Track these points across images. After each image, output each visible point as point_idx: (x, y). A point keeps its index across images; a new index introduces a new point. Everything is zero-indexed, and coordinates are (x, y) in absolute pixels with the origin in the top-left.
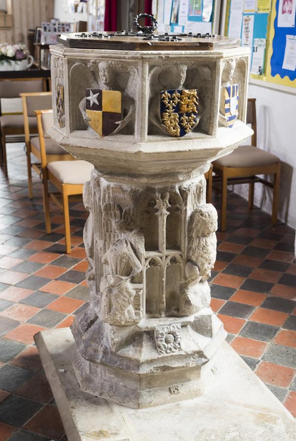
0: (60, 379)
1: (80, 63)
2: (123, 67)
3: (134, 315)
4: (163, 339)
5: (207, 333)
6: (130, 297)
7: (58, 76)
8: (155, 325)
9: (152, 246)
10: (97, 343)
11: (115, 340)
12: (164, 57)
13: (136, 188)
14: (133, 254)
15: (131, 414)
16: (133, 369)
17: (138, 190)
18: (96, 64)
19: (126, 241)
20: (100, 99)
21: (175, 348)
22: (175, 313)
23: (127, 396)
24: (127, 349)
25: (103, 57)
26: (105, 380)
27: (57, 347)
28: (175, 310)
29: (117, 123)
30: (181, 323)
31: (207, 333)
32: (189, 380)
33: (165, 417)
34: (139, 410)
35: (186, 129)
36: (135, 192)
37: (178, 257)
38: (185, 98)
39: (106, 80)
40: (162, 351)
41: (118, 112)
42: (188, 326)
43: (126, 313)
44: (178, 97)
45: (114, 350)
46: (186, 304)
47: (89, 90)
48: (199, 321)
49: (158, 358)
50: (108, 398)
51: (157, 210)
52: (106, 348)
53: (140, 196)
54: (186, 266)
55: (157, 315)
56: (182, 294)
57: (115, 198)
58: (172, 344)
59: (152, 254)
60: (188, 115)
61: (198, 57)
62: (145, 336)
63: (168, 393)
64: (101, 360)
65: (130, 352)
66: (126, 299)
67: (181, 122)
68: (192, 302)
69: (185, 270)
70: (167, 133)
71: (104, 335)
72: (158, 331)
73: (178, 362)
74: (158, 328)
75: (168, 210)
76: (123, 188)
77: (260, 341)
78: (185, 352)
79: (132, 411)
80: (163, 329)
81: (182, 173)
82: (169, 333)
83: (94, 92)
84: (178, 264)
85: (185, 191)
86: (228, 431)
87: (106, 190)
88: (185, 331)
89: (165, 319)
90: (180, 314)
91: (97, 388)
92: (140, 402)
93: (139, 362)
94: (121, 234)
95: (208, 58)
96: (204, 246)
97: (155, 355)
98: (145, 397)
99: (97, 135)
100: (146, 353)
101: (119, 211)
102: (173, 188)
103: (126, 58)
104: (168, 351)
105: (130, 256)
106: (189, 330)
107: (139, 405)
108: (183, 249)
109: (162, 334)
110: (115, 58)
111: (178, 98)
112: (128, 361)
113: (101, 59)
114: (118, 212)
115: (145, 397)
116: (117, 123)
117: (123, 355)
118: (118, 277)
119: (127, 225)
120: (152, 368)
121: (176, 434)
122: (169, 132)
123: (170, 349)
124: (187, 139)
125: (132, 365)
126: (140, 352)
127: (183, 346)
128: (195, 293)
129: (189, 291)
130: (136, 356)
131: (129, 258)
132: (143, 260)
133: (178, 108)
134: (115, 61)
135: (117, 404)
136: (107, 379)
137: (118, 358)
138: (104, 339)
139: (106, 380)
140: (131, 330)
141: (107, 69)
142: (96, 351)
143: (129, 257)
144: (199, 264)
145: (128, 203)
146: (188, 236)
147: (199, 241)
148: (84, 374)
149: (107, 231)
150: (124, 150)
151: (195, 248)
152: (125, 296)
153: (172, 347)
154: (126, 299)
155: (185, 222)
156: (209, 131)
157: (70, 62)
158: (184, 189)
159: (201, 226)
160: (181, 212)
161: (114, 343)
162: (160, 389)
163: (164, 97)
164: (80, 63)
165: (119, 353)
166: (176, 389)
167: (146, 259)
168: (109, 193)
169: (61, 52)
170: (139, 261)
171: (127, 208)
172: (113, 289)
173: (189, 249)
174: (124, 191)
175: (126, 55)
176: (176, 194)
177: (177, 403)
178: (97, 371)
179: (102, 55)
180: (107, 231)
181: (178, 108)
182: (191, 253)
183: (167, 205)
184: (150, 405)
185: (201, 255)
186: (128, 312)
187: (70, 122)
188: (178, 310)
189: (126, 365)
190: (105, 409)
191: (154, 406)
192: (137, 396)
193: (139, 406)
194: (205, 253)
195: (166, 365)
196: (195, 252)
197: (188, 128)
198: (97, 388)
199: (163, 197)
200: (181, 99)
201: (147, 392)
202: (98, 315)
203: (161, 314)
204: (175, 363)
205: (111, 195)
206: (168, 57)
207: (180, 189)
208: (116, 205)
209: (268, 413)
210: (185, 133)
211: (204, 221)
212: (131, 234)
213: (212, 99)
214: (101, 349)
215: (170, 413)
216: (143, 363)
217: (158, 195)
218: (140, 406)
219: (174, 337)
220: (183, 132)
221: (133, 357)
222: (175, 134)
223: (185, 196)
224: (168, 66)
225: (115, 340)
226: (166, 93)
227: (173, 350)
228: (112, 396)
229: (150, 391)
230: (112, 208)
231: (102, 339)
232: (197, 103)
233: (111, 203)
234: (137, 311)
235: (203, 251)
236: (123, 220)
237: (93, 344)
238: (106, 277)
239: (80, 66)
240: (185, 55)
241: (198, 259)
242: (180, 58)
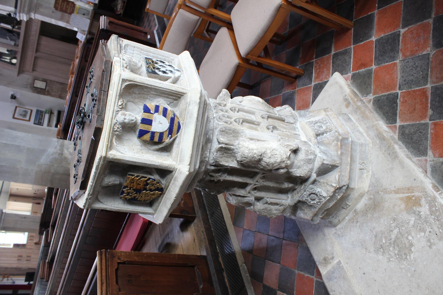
44: (129, 189)
73: (331, 202)
88: (318, 183)
95: (101, 168)
96: (267, 165)
104: (319, 204)
111: (130, 189)
115: (333, 221)
146: (251, 169)
166: (346, 205)
191: (343, 220)
201: (332, 218)
204: (330, 205)
209: (412, 194)
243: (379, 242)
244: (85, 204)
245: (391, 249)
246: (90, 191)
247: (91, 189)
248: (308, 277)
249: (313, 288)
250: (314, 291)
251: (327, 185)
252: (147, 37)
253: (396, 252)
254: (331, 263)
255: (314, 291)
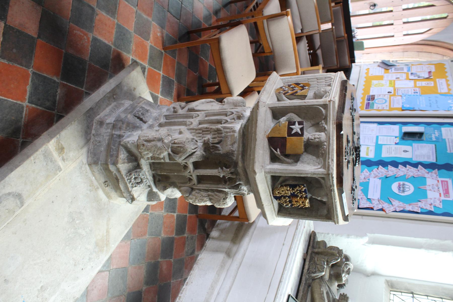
0: (102, 99)
1: (325, 115)
2: (322, 154)
3: (147, 157)
4: (136, 176)
5: (149, 199)
6: (158, 155)
7: (318, 81)
8: (144, 169)
9: (197, 165)
10: (126, 128)
11: (128, 144)
12: (331, 188)
13: (235, 154)
14: (188, 155)
15: (82, 162)
16: (111, 160)
17: (234, 156)
18: (324, 130)
19: (197, 148)
20: (296, 134)
21: (132, 184)
22: (157, 179)
23: (95, 155)
24: (125, 152)
25: (329, 138)
26: (103, 136)
27: (128, 84)
28: (159, 179)
29: (278, 150)
30: (150, 185)
31: (149, 199)
32: (116, 192)
33: (86, 185)
34: (87, 166)
35: (279, 200)
36: (233, 154)
37: (193, 183)
38: (302, 200)
39: (312, 139)
40: (128, 177)
41: (287, 151)
42: (150, 188)
43: (146, 152)
45: (122, 143)
46: (164, 186)
47: (303, 124)
48: (155, 194)
49: (122, 175)
50: (92, 141)
51: (222, 169)
52: (123, 136)
53: (231, 157)
54: (188, 188)
55: (153, 169)
56: (170, 185)
57: (226, 137)
58: (135, 181)
59: (191, 167)
60: (290, 202)
61: (333, 210)
62: (135, 164)
63: (103, 181)
64: (114, 134)
65: (123, 155)
66: (155, 152)
67: (285, 197)
68: (165, 191)
69: (186, 187)
70: (274, 188)
71: (133, 132)
72: (141, 172)
73: (124, 187)
74: (142, 172)
75: (224, 176)
76: (234, 144)
77: (164, 205)
78: (131, 190)
79: (85, 161)
80: (143, 175)
81: (251, 187)
82: (141, 179)
83: (302, 129)
84: (188, 183)
85: (239, 188)
86: (85, 228)
87: (232, 130)
88: (146, 187)
89: (151, 174)
90: (157, 183)
91: (97, 131)
92: (92, 165)
93: (116, 164)
94: (202, 143)
96: (203, 200)
97: (124, 172)
98: (96, 169)
99: (268, 131)
100: (123, 167)
101: (217, 141)
102: (240, 180)
103: (328, 159)
104: (129, 181)
105: (186, 153)
106: (147, 189)
107: (90, 165)
108: (198, 185)
109: (139, 175)
110: (329, 149)
111: (301, 196)
112: (116, 155)
113: (328, 135)
114: (216, 141)
115: (97, 167)
116: (278, 150)
117: (119, 151)
118: (170, 146)
119: (207, 146)
120: (115, 172)
121: (74, 198)
122: (275, 190)
123: (130, 182)
124: (272, 200)
125: (114, 158)
126: (124, 163)
127: (134, 188)
128: (172, 191)
129: (173, 188)
130: (120, 161)
131: (184, 153)
132: (185, 161)
133: (294, 195)
134: (326, 148)
135: (89, 149)
136: (104, 137)
137: (117, 147)
138: (130, 133)
139: (103, 137)
140: (138, 154)
141: (321, 141)
142: (120, 129)
143: (185, 152)
144: (191, 196)
145: (223, 149)
147: (206, 197)
148: (106, 117)
149: (203, 131)
150: (256, 160)
151: (201, 194)
152: (157, 151)
153: (132, 182)
154: (155, 152)
155: (217, 187)
156: (281, 213)
157: (325, 106)
158: (240, 187)
159: (217, 198)
160: (224, 185)
161: (126, 144)
162: (104, 175)
163: (300, 187)
164: (325, 115)
165: (121, 147)
166: (108, 185)
167: (186, 163)
168: (230, 132)
169: (333, 97)
170: (183, 159)
171: (220, 148)
172: (161, 141)
173: (200, 190)
174: (233, 144)
175: (331, 159)
176: (236, 182)
177: (99, 187)
178: (108, 129)
179: (331, 138)
180: (203, 131)
181: (294, 195)
182: (197, 191)
183: (226, 176)
184: (93, 172)
185: (197, 198)
186: (148, 154)
187: (277, 107)
188: (159, 181)
189: (113, 154)
190: (82, 142)
191: (93, 174)
192: (96, 163)
193: (90, 165)
194: (199, 201)
195: (120, 180)
196: (198, 194)
197: (280, 201)
198: (97, 131)
199: (232, 173)
200: (301, 197)
201: (100, 168)
202: (146, 124)
203: (153, 171)
204: (122, 185)
205: (229, 134)
206: (331, 191)
207: (240, 184)
208: (222, 138)
210: (277, 200)
211: (220, 201)
212: (202, 151)
213: (304, 216)
214: (121, 133)
215: (90, 186)
216: (116, 166)
217: (233, 170)
218: (90, 166)
219: (140, 182)
220: (276, 198)
221: (119, 158)
222: (274, 193)
223: (235, 188)
224: (326, 189)
225: (128, 144)
226: (305, 188)
227: (131, 184)
228: (93, 144)
229: (101, 170)
230: (219, 135)
231: (129, 132)
232: (299, 207)
233: (223, 134)
234: (150, 159)
235: (200, 199)
236: (211, 145)
237: (124, 126)
238: (169, 135)
239: (323, 115)
240: (335, 202)
241: (194, 196)
242: (332, 198)
243: (76, 216)
244: (333, 180)
245: (72, 230)
246: (334, 194)
247: (334, 197)
248: (26, 91)
249: (15, 100)
250: (12, 100)
251: (140, 192)
252: (312, 52)
253: (70, 235)
254: (59, 157)
255: (12, 100)
